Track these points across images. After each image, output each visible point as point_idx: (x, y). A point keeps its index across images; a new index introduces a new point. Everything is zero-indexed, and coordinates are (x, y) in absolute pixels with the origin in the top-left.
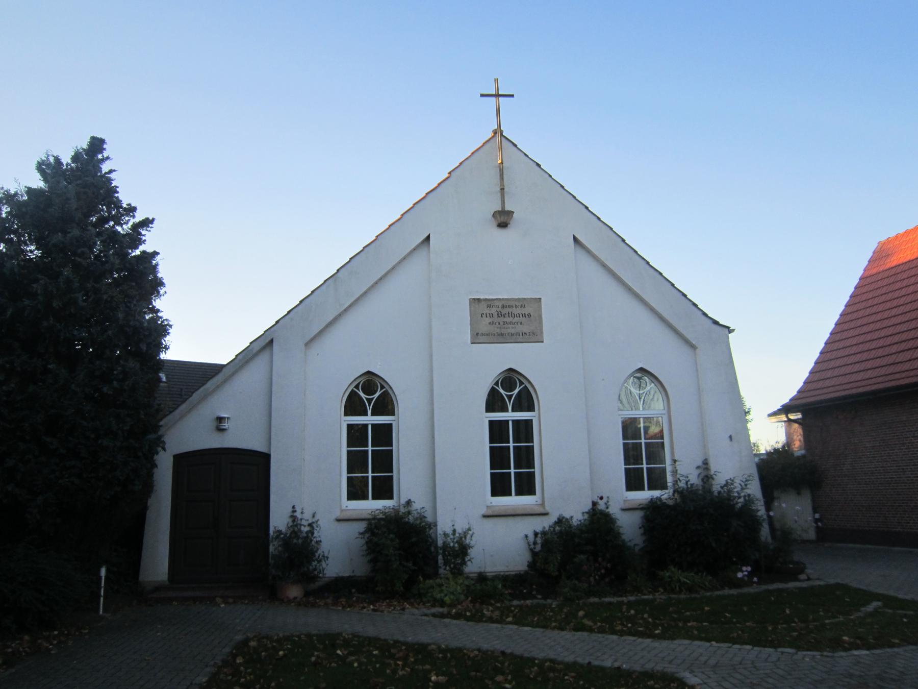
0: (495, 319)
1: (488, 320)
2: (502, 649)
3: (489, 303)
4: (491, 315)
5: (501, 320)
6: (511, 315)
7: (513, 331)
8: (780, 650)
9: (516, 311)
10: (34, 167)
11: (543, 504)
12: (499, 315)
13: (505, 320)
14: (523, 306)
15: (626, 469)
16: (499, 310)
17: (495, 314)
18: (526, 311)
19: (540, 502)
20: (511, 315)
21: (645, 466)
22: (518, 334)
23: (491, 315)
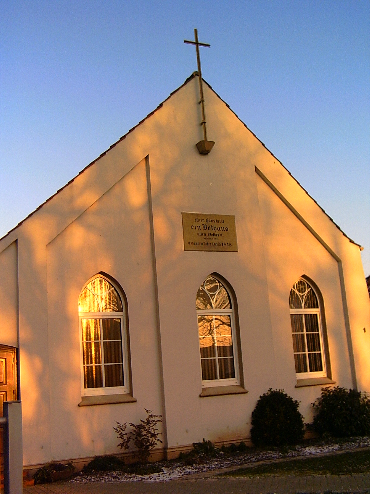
0: (203, 231)
1: (197, 231)
2: (193, 443)
3: (197, 217)
4: (199, 228)
5: (206, 232)
6: (213, 228)
7: (214, 241)
8: (263, 475)
9: (217, 225)
10: (215, 142)
11: (131, 394)
12: (205, 227)
13: (209, 232)
14: (222, 222)
15: (293, 335)
16: (204, 223)
17: (202, 227)
18: (223, 225)
19: (128, 392)
20: (213, 228)
21: (217, 358)
22: (219, 244)
23: (199, 228)
